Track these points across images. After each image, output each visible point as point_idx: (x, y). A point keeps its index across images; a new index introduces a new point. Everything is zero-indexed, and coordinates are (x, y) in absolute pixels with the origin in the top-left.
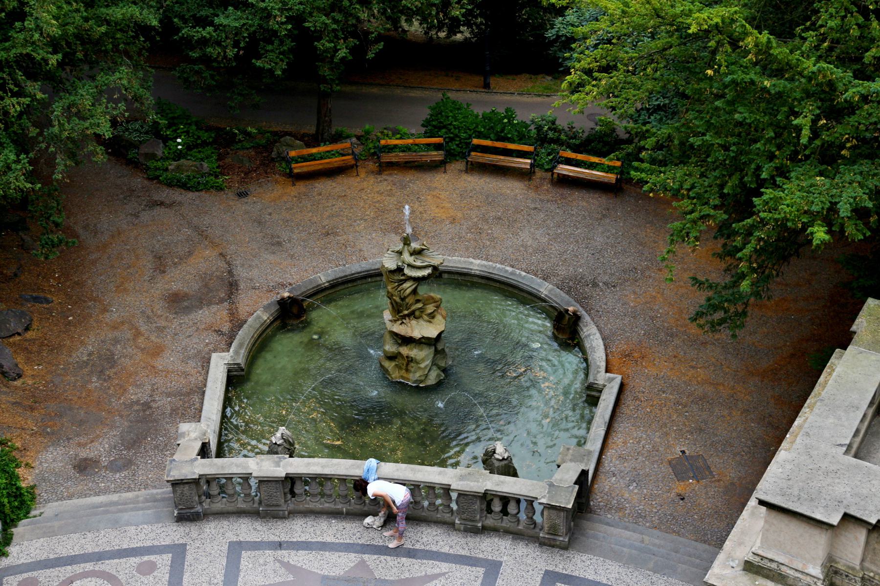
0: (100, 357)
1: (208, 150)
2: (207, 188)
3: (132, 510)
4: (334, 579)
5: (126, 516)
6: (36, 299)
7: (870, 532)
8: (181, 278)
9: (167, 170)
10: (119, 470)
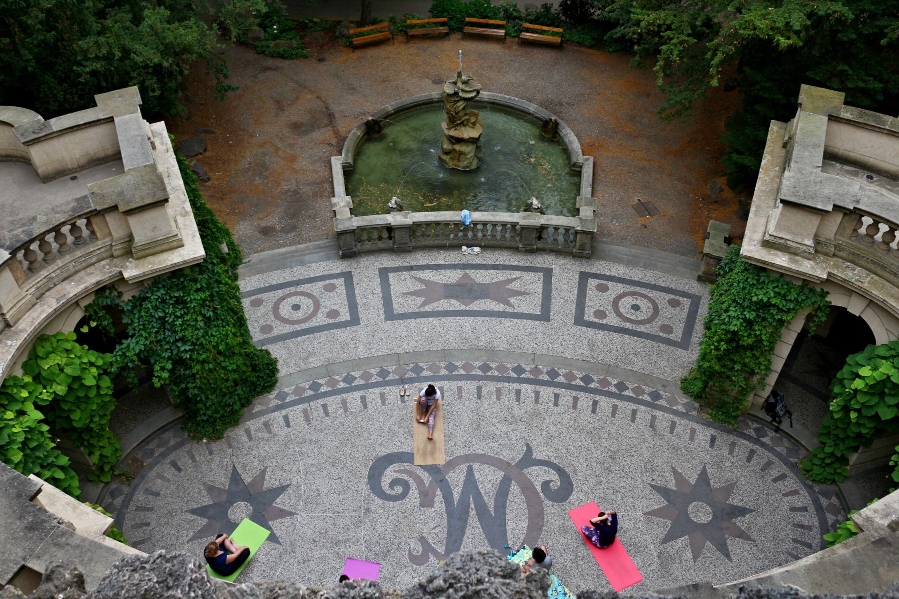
3: (309, 254)
4: (451, 285)
5: (307, 258)
6: (206, 132)
7: (845, 214)
8: (295, 114)
9: (268, 47)
10: (289, 231)
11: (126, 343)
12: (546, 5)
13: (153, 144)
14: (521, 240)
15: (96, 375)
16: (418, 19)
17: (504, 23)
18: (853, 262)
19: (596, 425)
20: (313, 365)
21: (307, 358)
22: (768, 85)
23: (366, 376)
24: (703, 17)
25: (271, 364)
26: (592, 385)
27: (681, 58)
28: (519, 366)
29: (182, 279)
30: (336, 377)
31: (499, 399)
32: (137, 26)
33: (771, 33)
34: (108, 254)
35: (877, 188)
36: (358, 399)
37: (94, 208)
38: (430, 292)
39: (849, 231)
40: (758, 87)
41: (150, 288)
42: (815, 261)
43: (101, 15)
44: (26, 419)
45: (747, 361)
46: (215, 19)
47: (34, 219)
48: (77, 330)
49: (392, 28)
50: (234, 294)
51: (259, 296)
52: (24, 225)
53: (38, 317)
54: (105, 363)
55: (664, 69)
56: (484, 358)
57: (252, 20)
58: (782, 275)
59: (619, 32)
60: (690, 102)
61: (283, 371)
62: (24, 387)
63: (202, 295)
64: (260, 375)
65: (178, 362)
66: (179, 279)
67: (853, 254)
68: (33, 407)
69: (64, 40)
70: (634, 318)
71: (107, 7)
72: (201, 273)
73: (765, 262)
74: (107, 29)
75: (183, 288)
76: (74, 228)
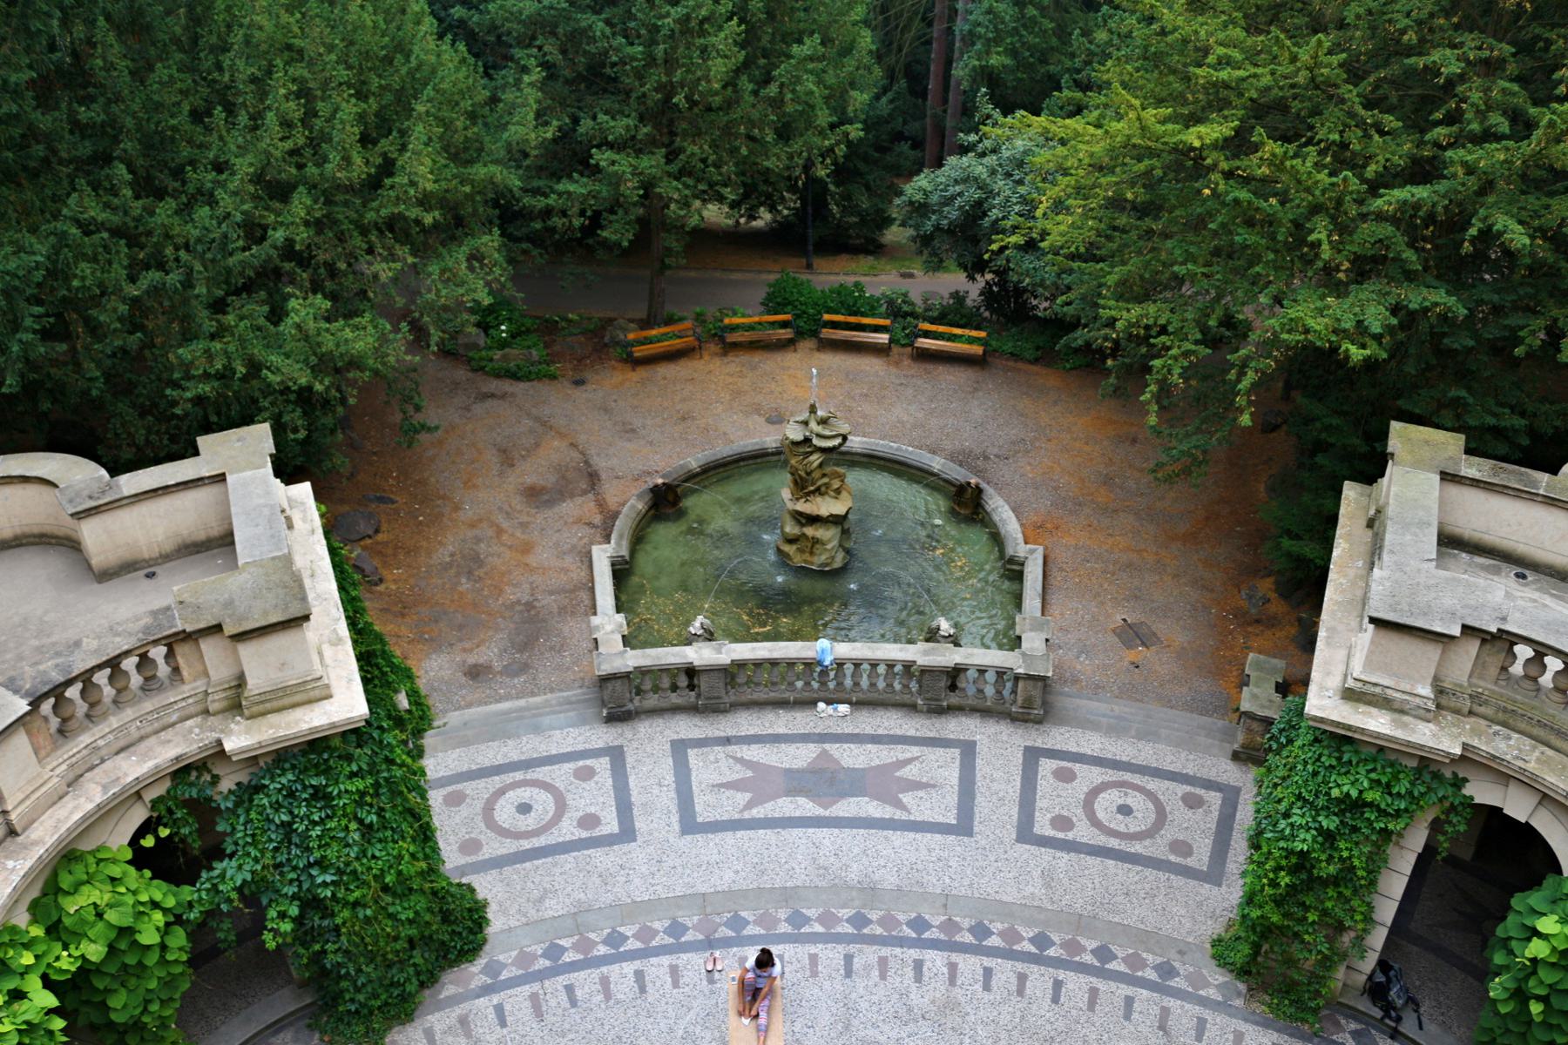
0: (463, 557)
1: (533, 338)
2: (539, 377)
5: (546, 720)
6: (381, 500)
7: (1484, 641)
8: (533, 471)
9: (491, 360)
11: (219, 866)
12: (957, 292)
13: (288, 519)
14: (920, 693)
15: (161, 924)
16: (743, 316)
17: (887, 322)
18: (1504, 724)
19: (1060, 1025)
20: (551, 913)
21: (541, 900)
22: (1335, 421)
23: (645, 934)
24: (1219, 311)
25: (477, 910)
26: (1051, 952)
27: (1186, 380)
28: (919, 917)
29: (326, 756)
30: (592, 936)
31: (883, 976)
32: (276, 324)
33: (1334, 338)
34: (200, 707)
35: (1536, 595)
36: (631, 976)
37: (180, 628)
38: (761, 783)
39: (1493, 671)
40: (1318, 425)
41: (268, 770)
42: (1438, 723)
43: (219, 307)
44: (24, 1008)
45: (1329, 904)
46: (405, 314)
47: (77, 644)
48: (134, 842)
49: (698, 330)
50: (415, 782)
51: (459, 787)
52: (58, 654)
53: (67, 818)
54: (178, 904)
55: (1158, 398)
56: (857, 903)
57: (465, 316)
58: (1381, 749)
59: (1080, 337)
60: (1205, 452)
61: (497, 923)
62: (27, 946)
63: (359, 784)
64: (456, 929)
65: (311, 903)
66: (320, 754)
67: (1505, 710)
68: (39, 984)
69: (154, 346)
70: (1122, 828)
71: (227, 294)
72: (359, 746)
73: (1349, 728)
74: (226, 330)
75: (327, 771)
76: (144, 661)
